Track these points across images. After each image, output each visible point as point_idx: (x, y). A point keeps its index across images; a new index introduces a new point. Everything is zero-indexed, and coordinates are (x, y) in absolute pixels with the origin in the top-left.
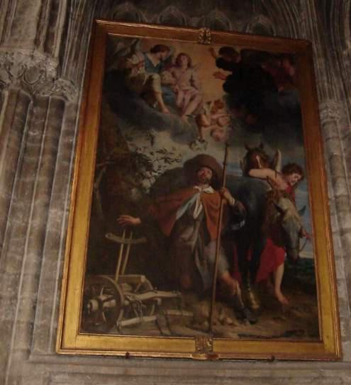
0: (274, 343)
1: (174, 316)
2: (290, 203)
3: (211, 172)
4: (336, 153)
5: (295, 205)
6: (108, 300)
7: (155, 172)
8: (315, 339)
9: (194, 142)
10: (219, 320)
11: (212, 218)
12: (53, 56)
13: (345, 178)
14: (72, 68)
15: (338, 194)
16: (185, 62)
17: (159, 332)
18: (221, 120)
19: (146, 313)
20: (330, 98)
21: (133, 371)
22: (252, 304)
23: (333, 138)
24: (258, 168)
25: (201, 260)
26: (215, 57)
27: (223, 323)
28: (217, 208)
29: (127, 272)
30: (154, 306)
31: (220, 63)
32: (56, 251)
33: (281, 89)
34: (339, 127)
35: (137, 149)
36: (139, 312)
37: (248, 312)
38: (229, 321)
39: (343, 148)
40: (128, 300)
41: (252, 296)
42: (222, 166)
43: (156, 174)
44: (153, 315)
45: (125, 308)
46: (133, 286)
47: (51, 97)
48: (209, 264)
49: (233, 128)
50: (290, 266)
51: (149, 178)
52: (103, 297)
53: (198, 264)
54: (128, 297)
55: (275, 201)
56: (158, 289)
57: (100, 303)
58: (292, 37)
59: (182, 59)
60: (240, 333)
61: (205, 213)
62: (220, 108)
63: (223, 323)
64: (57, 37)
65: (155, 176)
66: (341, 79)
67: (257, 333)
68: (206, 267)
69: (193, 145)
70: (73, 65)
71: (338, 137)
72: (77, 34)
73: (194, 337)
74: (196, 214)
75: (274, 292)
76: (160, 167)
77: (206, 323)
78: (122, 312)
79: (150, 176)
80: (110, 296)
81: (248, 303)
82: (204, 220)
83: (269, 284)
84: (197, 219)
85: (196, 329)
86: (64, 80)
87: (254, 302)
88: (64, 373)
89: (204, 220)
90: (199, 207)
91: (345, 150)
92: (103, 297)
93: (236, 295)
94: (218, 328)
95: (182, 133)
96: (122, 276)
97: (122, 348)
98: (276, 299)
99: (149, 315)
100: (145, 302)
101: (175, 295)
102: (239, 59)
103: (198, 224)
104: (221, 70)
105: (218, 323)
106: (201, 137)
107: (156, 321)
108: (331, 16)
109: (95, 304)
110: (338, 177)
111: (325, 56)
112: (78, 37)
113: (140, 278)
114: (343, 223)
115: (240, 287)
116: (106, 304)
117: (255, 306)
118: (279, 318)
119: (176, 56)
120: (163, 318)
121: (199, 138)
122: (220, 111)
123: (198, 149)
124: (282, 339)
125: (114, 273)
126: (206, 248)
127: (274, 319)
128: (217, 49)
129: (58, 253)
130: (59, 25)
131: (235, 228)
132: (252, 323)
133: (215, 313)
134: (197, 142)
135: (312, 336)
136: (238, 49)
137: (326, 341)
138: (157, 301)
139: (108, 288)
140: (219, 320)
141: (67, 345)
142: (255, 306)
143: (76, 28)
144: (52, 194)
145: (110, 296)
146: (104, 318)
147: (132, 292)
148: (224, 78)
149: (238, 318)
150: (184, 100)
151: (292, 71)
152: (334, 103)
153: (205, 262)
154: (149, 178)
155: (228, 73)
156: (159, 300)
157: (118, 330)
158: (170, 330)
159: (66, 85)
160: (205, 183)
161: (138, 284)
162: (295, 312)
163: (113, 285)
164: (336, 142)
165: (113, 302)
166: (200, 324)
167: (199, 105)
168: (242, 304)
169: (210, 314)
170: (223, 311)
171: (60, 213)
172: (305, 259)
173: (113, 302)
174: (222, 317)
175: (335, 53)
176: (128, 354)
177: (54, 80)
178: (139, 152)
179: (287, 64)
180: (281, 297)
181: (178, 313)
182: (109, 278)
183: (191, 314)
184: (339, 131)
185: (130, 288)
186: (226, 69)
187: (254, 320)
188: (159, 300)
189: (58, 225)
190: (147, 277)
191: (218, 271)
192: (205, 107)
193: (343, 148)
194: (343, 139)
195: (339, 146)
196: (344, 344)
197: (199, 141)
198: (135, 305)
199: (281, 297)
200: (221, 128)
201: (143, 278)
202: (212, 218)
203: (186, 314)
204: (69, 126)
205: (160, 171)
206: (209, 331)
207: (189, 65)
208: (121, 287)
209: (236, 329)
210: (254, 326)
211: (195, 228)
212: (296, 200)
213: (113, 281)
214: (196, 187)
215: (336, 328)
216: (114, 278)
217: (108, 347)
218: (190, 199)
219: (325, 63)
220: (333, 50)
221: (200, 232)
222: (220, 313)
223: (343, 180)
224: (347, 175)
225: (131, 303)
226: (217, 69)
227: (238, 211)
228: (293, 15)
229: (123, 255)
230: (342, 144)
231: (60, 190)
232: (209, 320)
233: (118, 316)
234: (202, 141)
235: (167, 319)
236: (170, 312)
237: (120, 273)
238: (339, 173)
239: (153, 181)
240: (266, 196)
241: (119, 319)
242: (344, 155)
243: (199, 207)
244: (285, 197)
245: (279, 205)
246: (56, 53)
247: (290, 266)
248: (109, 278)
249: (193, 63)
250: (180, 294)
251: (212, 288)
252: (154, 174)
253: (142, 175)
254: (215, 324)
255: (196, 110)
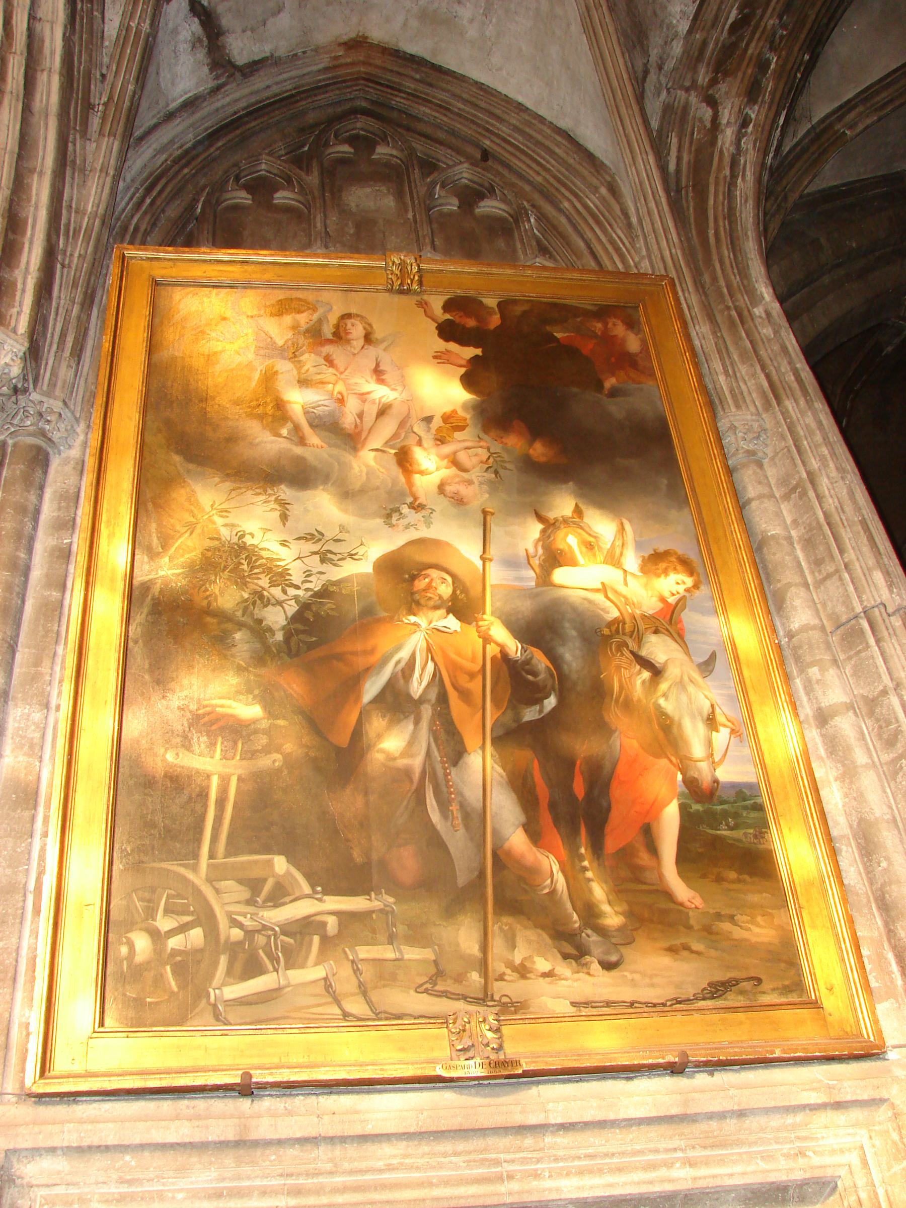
0: (679, 1017)
1: (378, 962)
2: (674, 645)
3: (449, 579)
4: (775, 530)
5: (687, 651)
6: (183, 929)
7: (297, 587)
8: (793, 998)
9: (397, 510)
10: (510, 965)
11: (465, 695)
12: (15, 331)
13: (806, 585)
14: (65, 373)
15: (795, 625)
16: (357, 331)
17: (337, 1011)
18: (462, 457)
19: (293, 959)
20: (738, 407)
21: (264, 1129)
22: (600, 915)
23: (760, 497)
24: (573, 563)
25: (443, 805)
26: (434, 320)
27: (523, 971)
28: (477, 667)
29: (233, 849)
30: (316, 939)
31: (447, 331)
32: (27, 814)
33: (610, 382)
34: (772, 473)
35: (243, 536)
36: (274, 959)
37: (592, 938)
38: (542, 964)
39: (789, 522)
40: (241, 926)
41: (599, 892)
42: (479, 563)
43: (300, 593)
44: (316, 964)
45: (234, 948)
46: (254, 885)
47: (10, 442)
48: (467, 816)
49: (496, 472)
50: (697, 807)
51: (280, 603)
52: (164, 924)
53: (435, 816)
54: (240, 918)
55: (632, 644)
56: (326, 892)
57: (156, 935)
58: (620, 266)
59: (349, 326)
60: (578, 999)
61: (441, 680)
62: (461, 428)
63: (523, 971)
64: (24, 291)
65: (296, 598)
66: (758, 368)
67: (628, 994)
68: (459, 821)
69: (395, 517)
70: (69, 366)
71: (772, 496)
72: (78, 299)
73: (443, 1020)
74: (417, 686)
75: (661, 876)
76: (308, 574)
77: (475, 977)
78: (223, 960)
79: (282, 597)
80: (188, 918)
81: (590, 913)
82: (443, 698)
83: (644, 858)
84: (421, 700)
85: (445, 994)
86: (45, 399)
87: (606, 908)
88: (53, 1150)
89: (443, 698)
90: (423, 669)
91: (795, 522)
92: (164, 924)
93: (553, 892)
94: (510, 988)
95: (363, 491)
96: (220, 860)
97: (228, 1061)
98: (668, 895)
99: (302, 966)
100: (287, 929)
101: (376, 904)
102: (495, 321)
103: (427, 712)
104: (453, 346)
105: (510, 975)
106: (416, 499)
107: (326, 979)
108: (712, 240)
109: (142, 943)
110: (789, 585)
111: (711, 318)
112: (82, 305)
113: (270, 863)
114: (819, 693)
115: (563, 870)
116: (174, 943)
117: (612, 918)
118: (686, 948)
119: (333, 319)
120: (346, 971)
121: (409, 500)
122: (458, 435)
123: (407, 527)
124: (702, 1004)
125: (196, 856)
126: (453, 771)
127: (672, 950)
128: (437, 303)
129: (33, 819)
130: (28, 263)
131: (530, 714)
132: (608, 966)
133: (497, 945)
134: (405, 510)
135: (786, 990)
136: (491, 302)
137: (828, 1002)
138: (324, 924)
139: (179, 896)
140: (510, 965)
141: (60, 1063)
142: (612, 918)
143: (75, 285)
144: (17, 670)
145: (188, 918)
146: (173, 983)
147: (250, 902)
148: (463, 362)
149: (565, 956)
150: (360, 416)
151: (633, 344)
152: (749, 417)
153: (454, 807)
154: (280, 603)
155: (470, 352)
156: (332, 923)
157: (217, 1016)
158: (369, 1003)
159: (51, 411)
160: (436, 608)
161: (265, 880)
162: (726, 926)
163: (194, 886)
164: (768, 504)
165: (196, 935)
166: (459, 979)
167: (402, 424)
168: (575, 917)
169: (484, 947)
170: (520, 941)
171: (37, 716)
172: (733, 785)
173: (196, 935)
174: (518, 958)
175: (734, 313)
176: (247, 1075)
177: (16, 390)
178: (249, 540)
179: (619, 329)
180: (681, 890)
181: (388, 953)
182: (182, 870)
183: (427, 954)
184: (773, 482)
185: (246, 894)
186: (463, 342)
187: (614, 958)
188: (332, 923)
189: (32, 747)
190: (291, 860)
191: (495, 832)
192: (419, 428)
193: (789, 522)
194: (786, 497)
195: (779, 514)
196: (882, 1008)
197: (411, 506)
198: (260, 940)
199: (681, 890)
200: (465, 475)
201: (280, 864)
202: (465, 695)
203: (412, 953)
204: (59, 509)
205: (308, 585)
206: (484, 998)
207: (368, 338)
208: (217, 891)
209: (562, 987)
210: (614, 973)
211: (417, 722)
212: (687, 638)
213: (190, 876)
214: (412, 619)
215: (852, 960)
216: (195, 868)
217: (186, 1063)
218: (398, 648)
219: (714, 333)
220: (728, 308)
221: (433, 733)
222: (512, 945)
223: (802, 592)
224: (810, 579)
225: (250, 934)
226: (441, 345)
227: (535, 674)
228: (617, 249)
229: (213, 828)
230: (785, 513)
231: (37, 663)
232: (483, 965)
233: (212, 976)
234: (417, 507)
235: (357, 971)
236: (364, 952)
237: (212, 856)
238: (788, 576)
239: (292, 608)
240: (606, 631)
241: (216, 982)
242: (794, 533)
243: (423, 669)
244: (656, 632)
245: (643, 653)
246: (23, 325)
247: (697, 807)
248: (182, 870)
249: (378, 334)
250: (391, 900)
251: (482, 874)
252: (292, 592)
253: (261, 597)
254: (501, 978)
255: (395, 436)
